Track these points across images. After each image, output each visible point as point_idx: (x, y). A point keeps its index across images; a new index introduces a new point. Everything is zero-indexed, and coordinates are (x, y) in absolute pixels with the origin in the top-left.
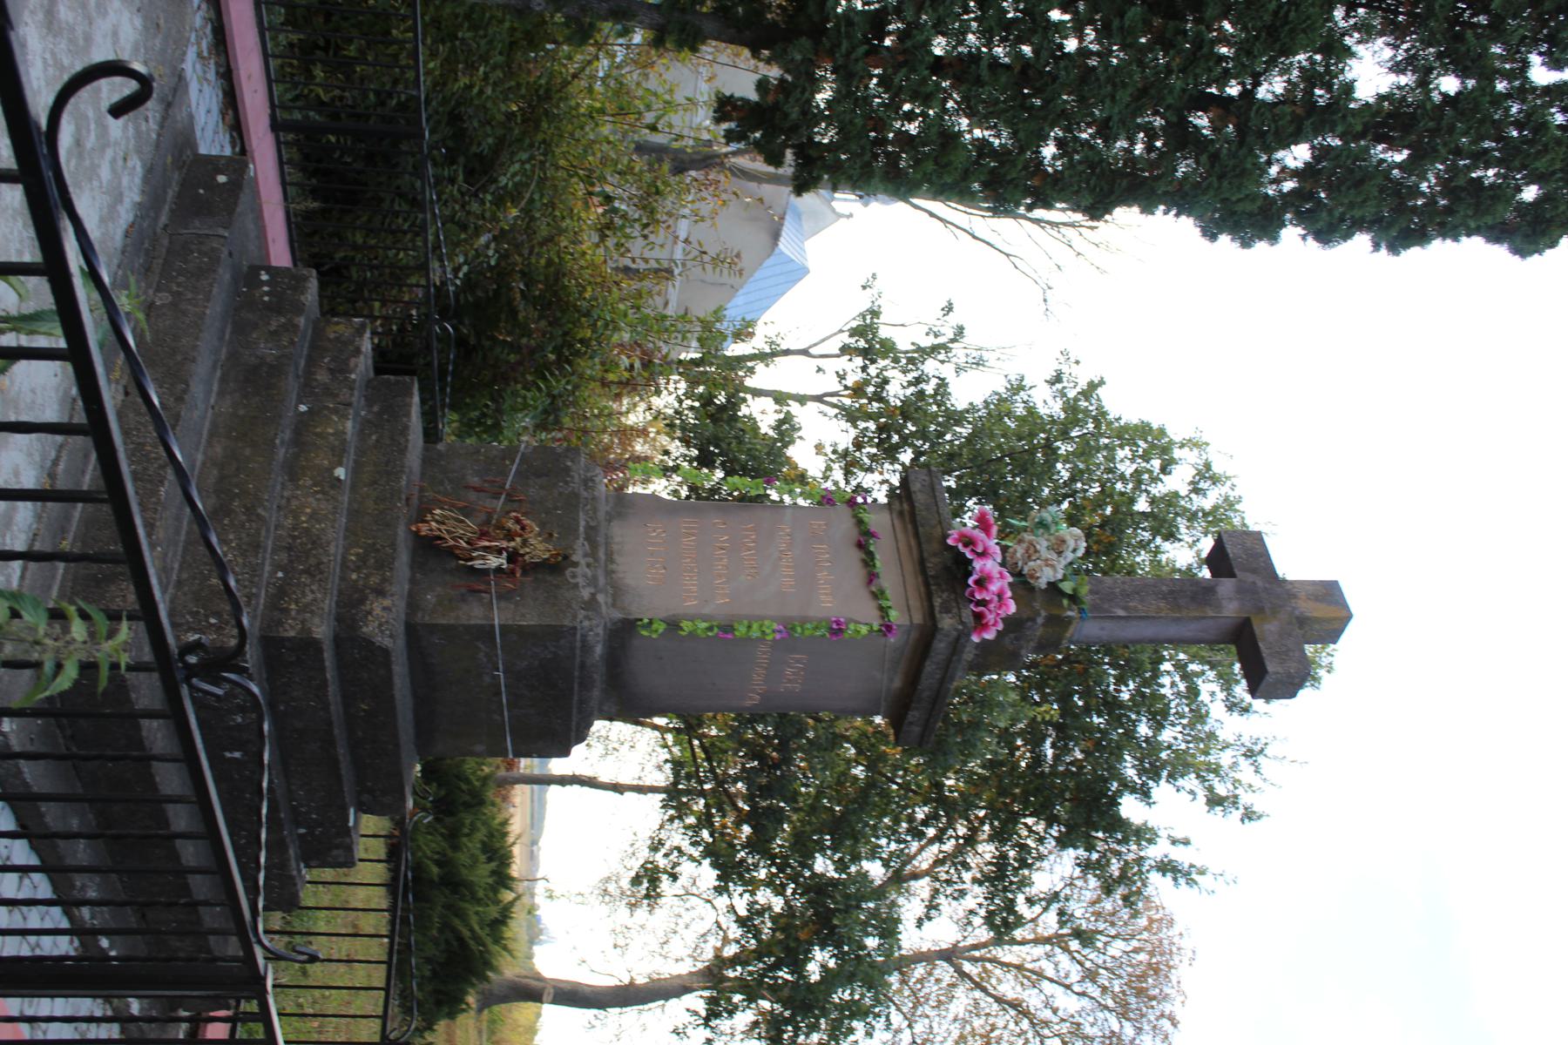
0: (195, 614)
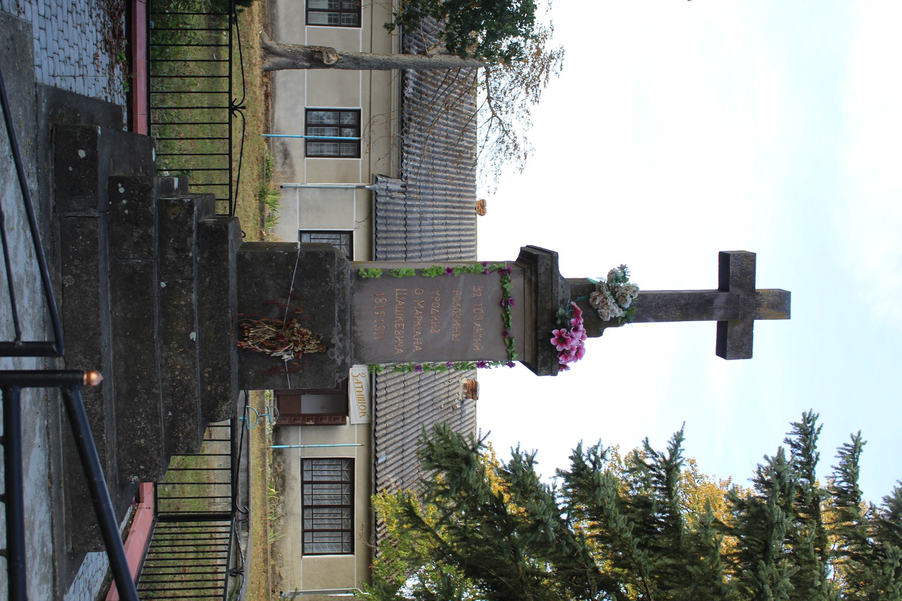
0: (132, 464)
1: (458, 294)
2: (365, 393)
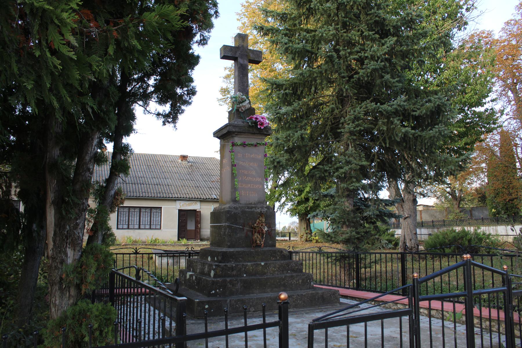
1: (241, 163)
2: (187, 203)
